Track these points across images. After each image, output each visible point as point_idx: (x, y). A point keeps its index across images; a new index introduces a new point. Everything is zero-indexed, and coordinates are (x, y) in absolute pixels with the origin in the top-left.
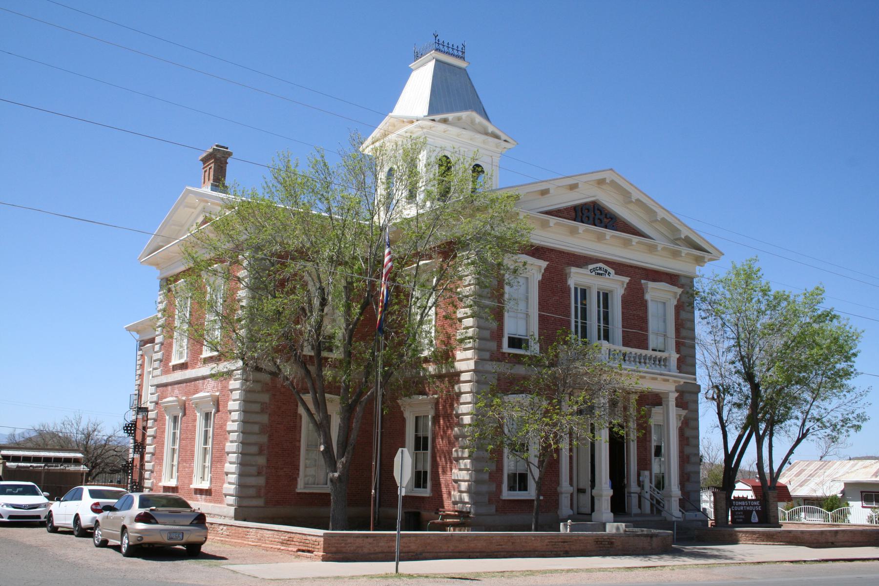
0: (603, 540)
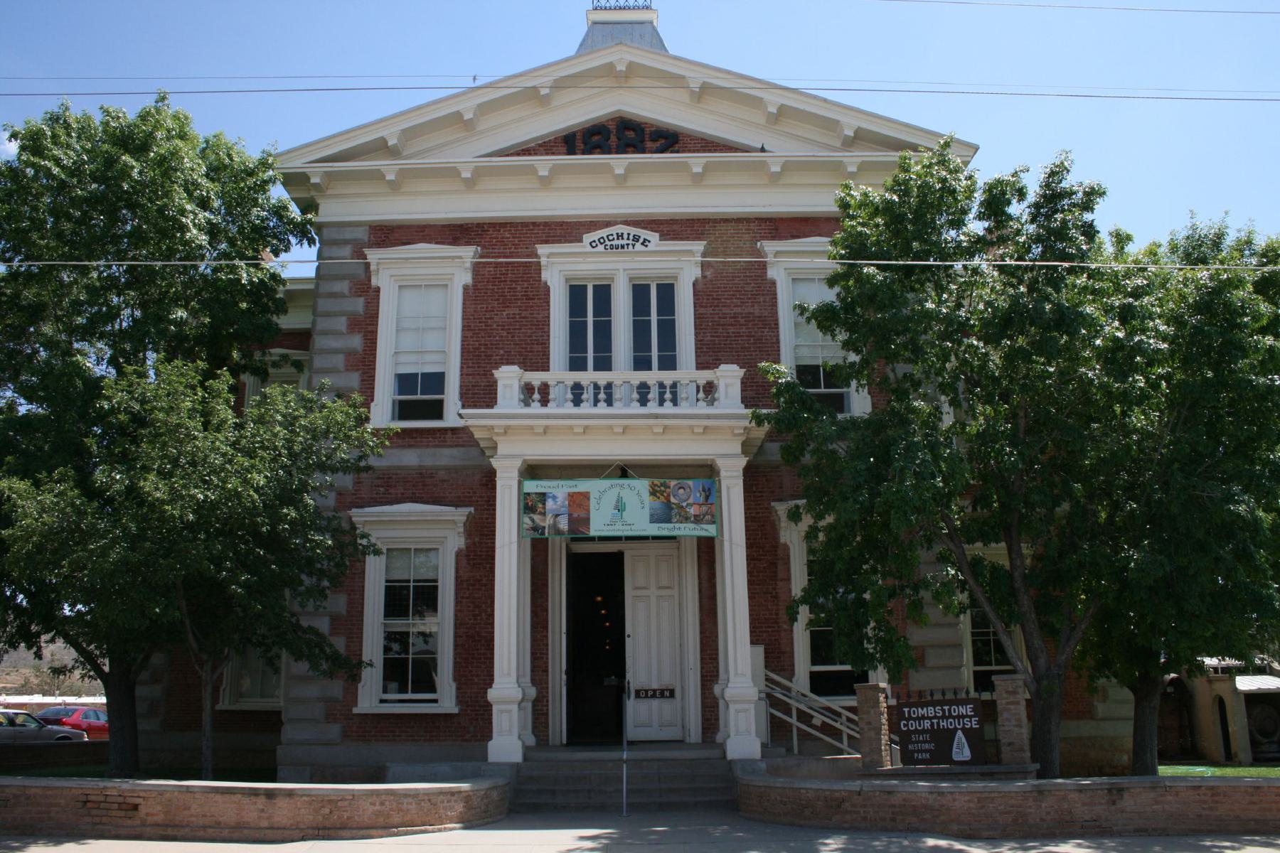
0: (102, 799)
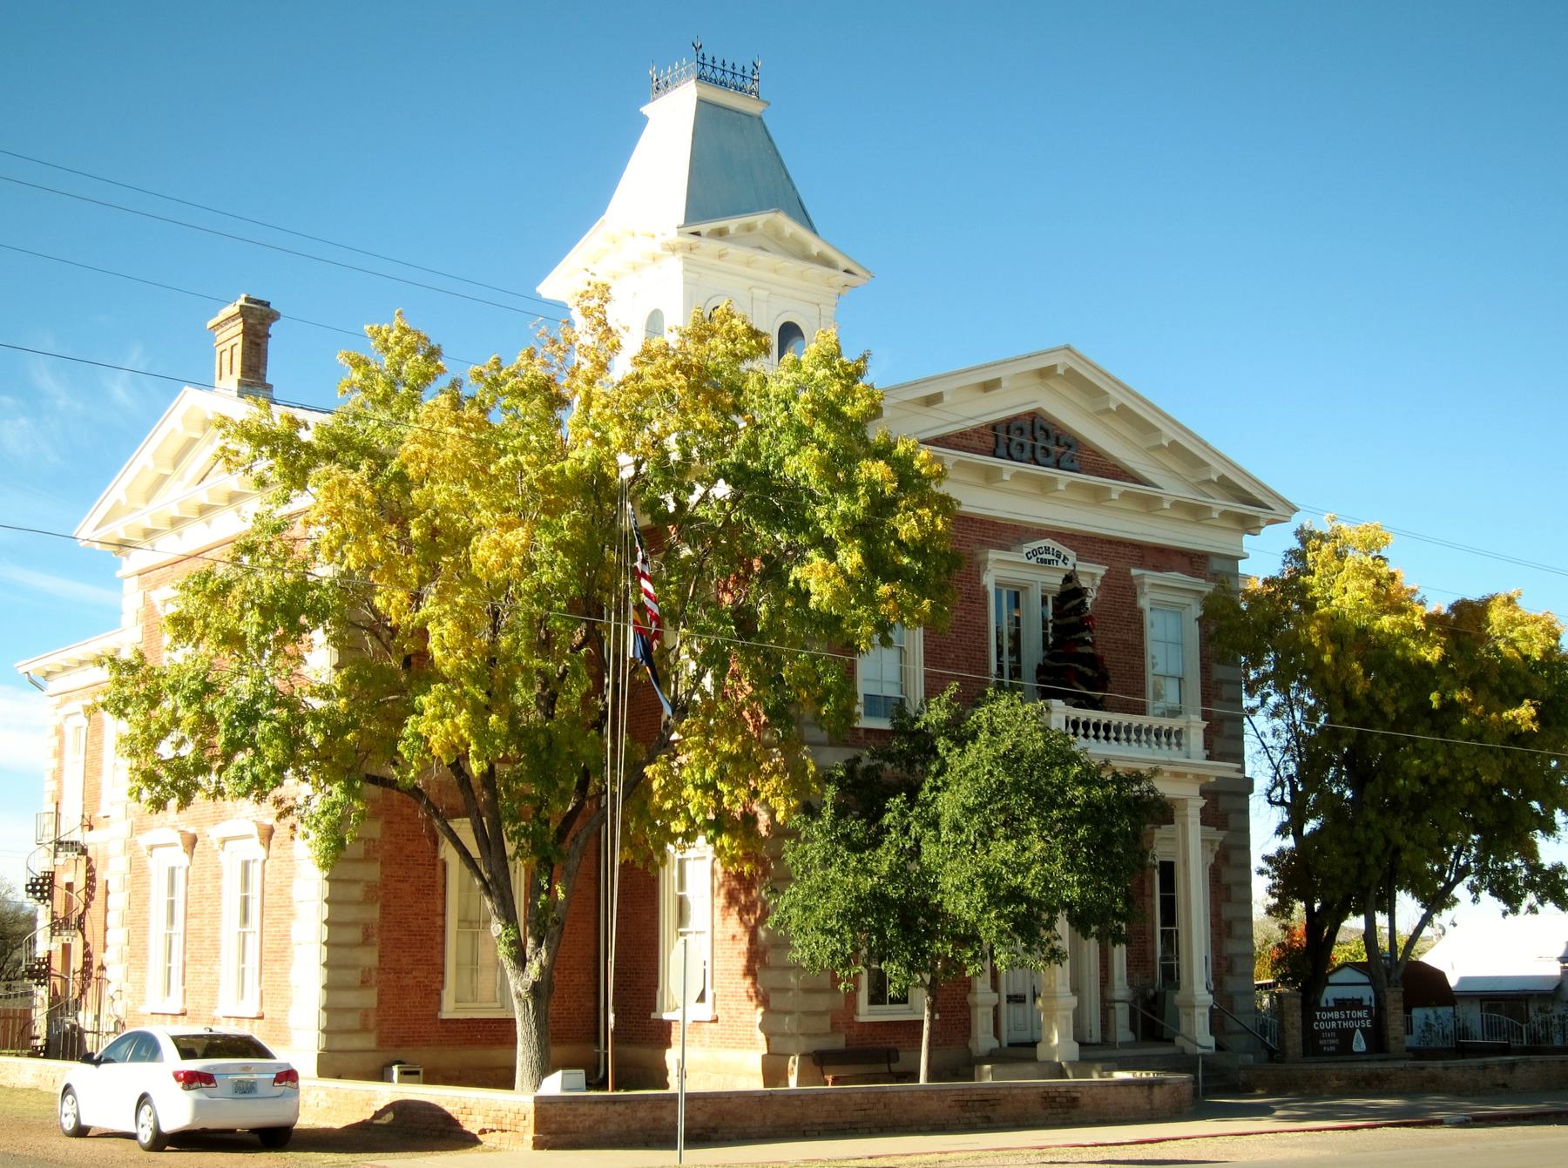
0: (1056, 1094)
